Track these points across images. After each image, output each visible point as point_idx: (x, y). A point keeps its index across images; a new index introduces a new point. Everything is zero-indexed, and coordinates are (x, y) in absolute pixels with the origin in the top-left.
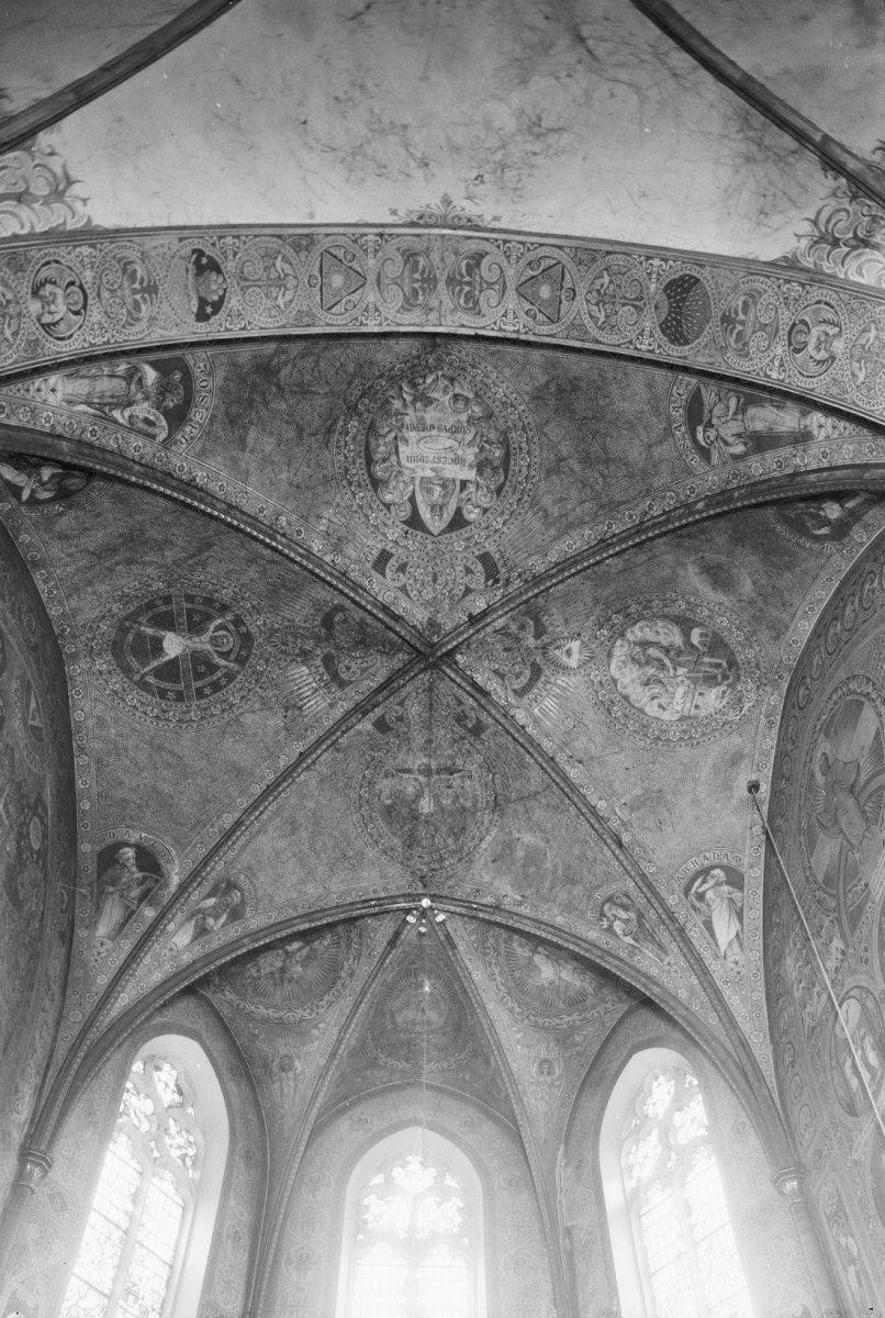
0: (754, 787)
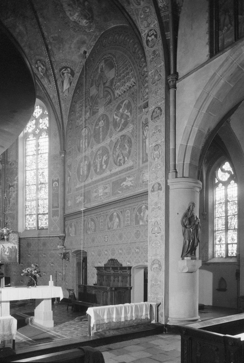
0: (85, 52)
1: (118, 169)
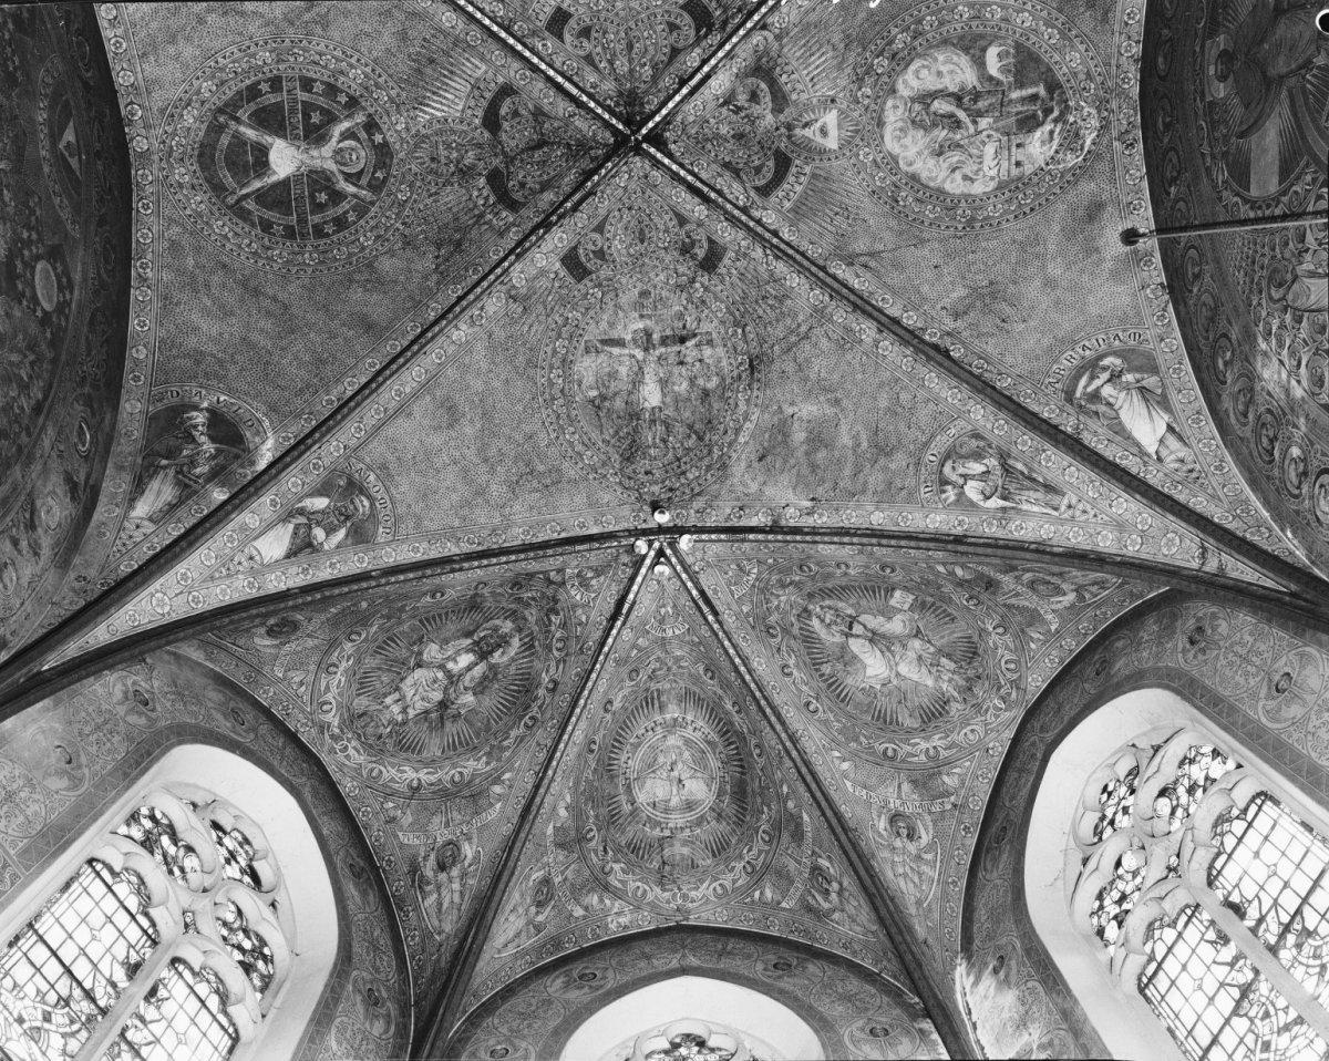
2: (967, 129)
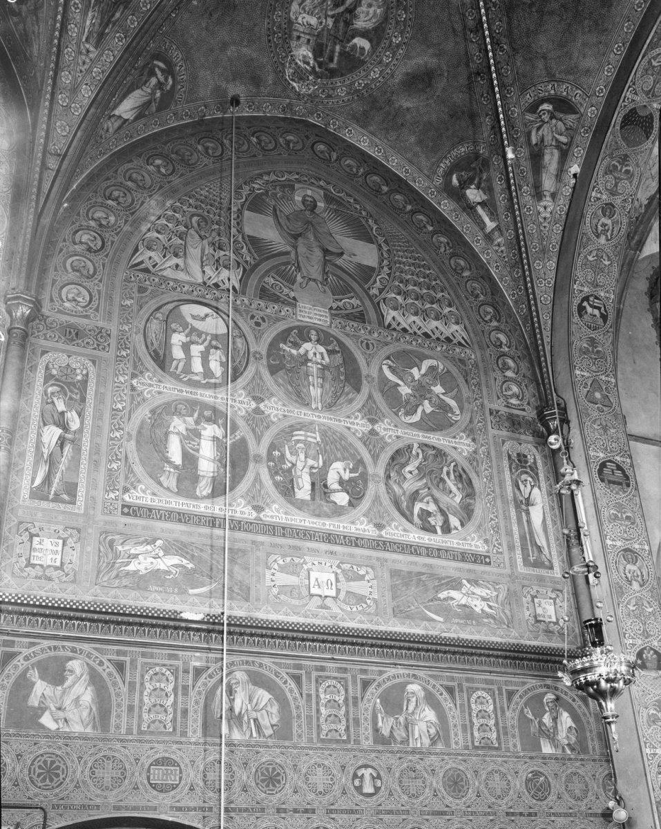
0: (235, 101)
1: (415, 536)
2: (331, 10)
